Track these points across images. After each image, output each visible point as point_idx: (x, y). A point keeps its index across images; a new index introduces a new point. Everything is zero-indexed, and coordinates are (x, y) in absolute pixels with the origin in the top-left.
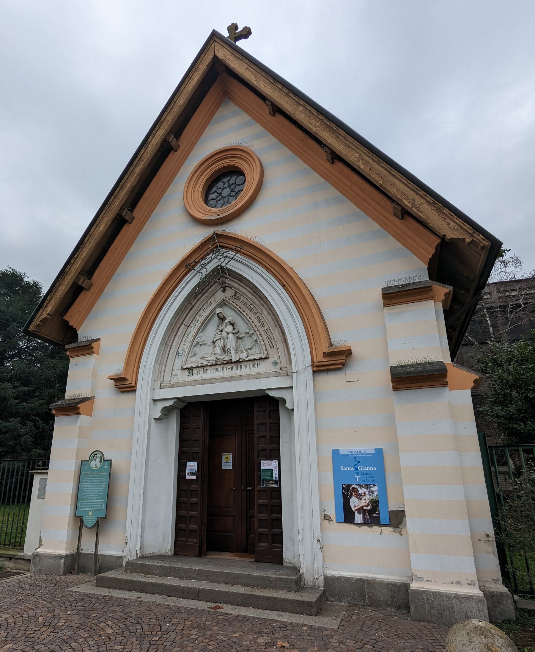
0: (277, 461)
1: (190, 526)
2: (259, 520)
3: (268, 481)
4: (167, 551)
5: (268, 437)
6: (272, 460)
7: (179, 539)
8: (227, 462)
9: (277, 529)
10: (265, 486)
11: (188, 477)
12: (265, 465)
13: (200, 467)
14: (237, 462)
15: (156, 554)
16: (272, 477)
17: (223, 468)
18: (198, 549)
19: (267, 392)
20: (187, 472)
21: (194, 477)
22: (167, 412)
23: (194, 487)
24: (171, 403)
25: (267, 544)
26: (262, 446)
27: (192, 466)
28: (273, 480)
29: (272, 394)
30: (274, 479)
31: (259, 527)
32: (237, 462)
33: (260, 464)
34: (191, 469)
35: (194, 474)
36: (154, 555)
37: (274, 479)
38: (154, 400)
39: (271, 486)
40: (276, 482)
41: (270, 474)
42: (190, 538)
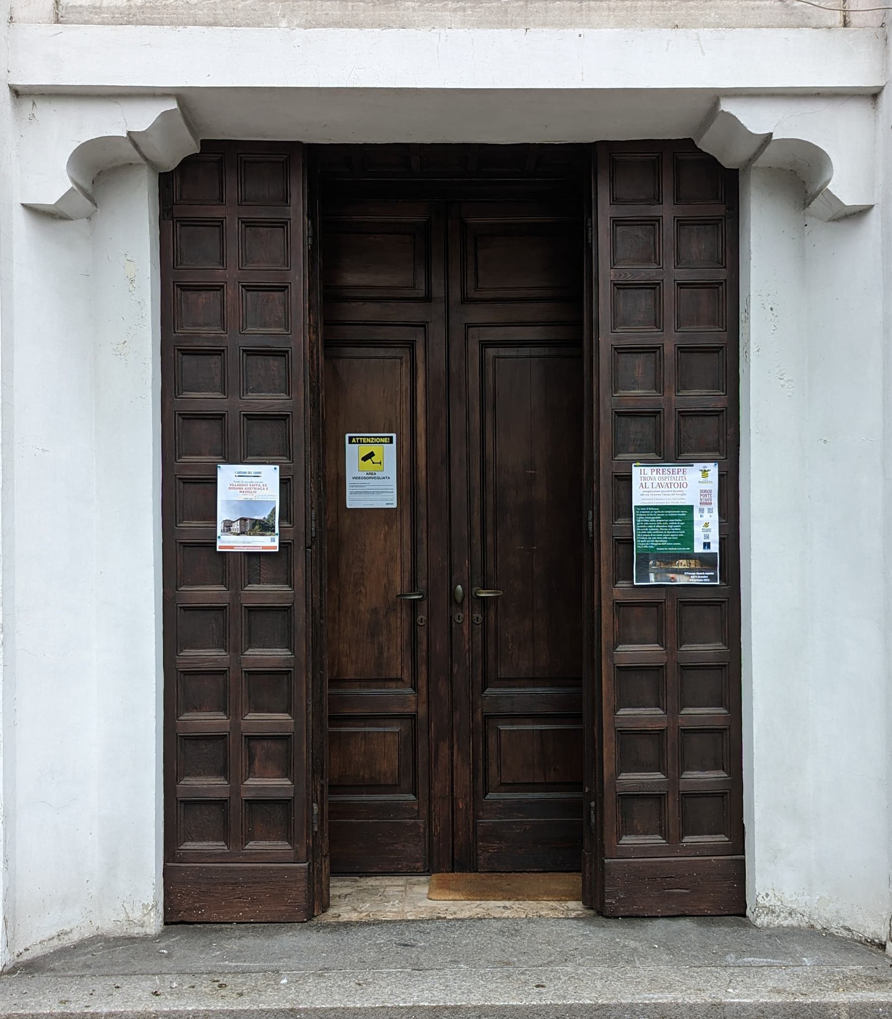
0: (713, 470)
1: (251, 782)
2: (623, 734)
3: (668, 559)
4: (137, 915)
5: (669, 349)
6: (689, 462)
7: (190, 846)
8: (371, 475)
9: (704, 769)
10: (652, 580)
11: (227, 542)
12: (653, 486)
13: (705, 455)
14: (422, 473)
15: (75, 937)
16: (688, 538)
17: (353, 501)
18: (302, 886)
19: (727, 106)
20: (223, 515)
21: (269, 543)
22: (99, 170)
23: (266, 590)
24: (142, 118)
25: (656, 840)
26: (638, 394)
27: (249, 490)
28: (690, 556)
29: (756, 120)
30: (698, 549)
31: (624, 767)
32: (422, 473)
33: (629, 478)
34: (249, 503)
35: (264, 527)
36: (66, 942)
37: (698, 549)
38: (17, 93)
39: (682, 580)
40: (705, 561)
41: (676, 526)
42: (251, 837)
